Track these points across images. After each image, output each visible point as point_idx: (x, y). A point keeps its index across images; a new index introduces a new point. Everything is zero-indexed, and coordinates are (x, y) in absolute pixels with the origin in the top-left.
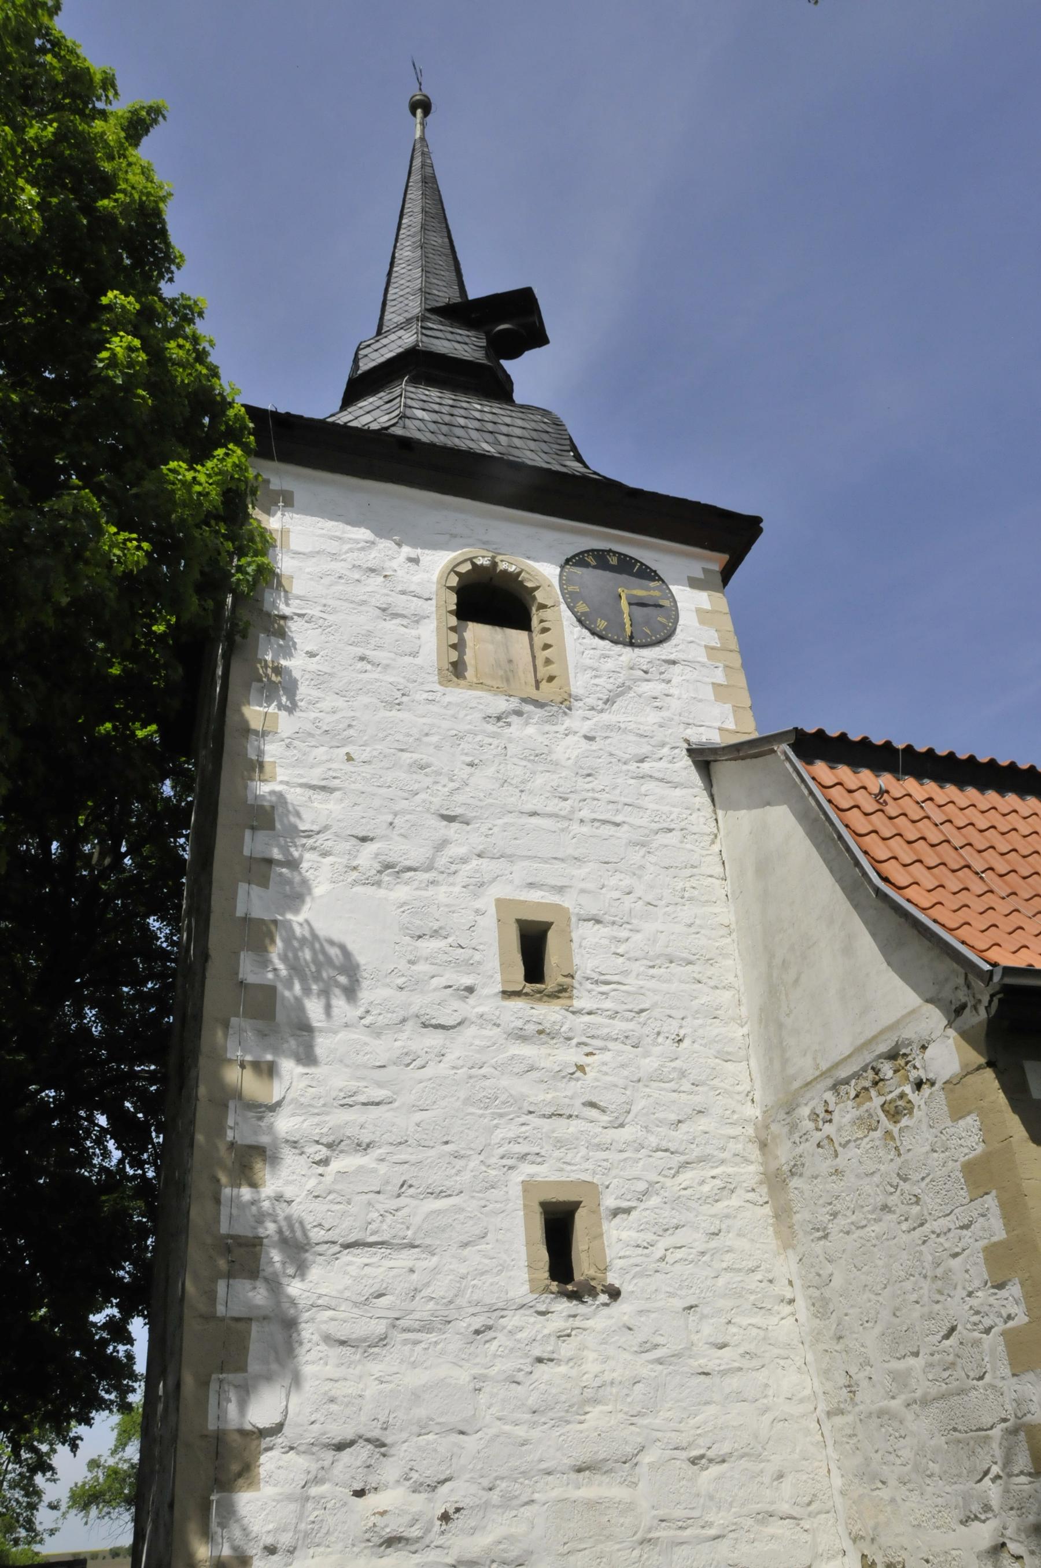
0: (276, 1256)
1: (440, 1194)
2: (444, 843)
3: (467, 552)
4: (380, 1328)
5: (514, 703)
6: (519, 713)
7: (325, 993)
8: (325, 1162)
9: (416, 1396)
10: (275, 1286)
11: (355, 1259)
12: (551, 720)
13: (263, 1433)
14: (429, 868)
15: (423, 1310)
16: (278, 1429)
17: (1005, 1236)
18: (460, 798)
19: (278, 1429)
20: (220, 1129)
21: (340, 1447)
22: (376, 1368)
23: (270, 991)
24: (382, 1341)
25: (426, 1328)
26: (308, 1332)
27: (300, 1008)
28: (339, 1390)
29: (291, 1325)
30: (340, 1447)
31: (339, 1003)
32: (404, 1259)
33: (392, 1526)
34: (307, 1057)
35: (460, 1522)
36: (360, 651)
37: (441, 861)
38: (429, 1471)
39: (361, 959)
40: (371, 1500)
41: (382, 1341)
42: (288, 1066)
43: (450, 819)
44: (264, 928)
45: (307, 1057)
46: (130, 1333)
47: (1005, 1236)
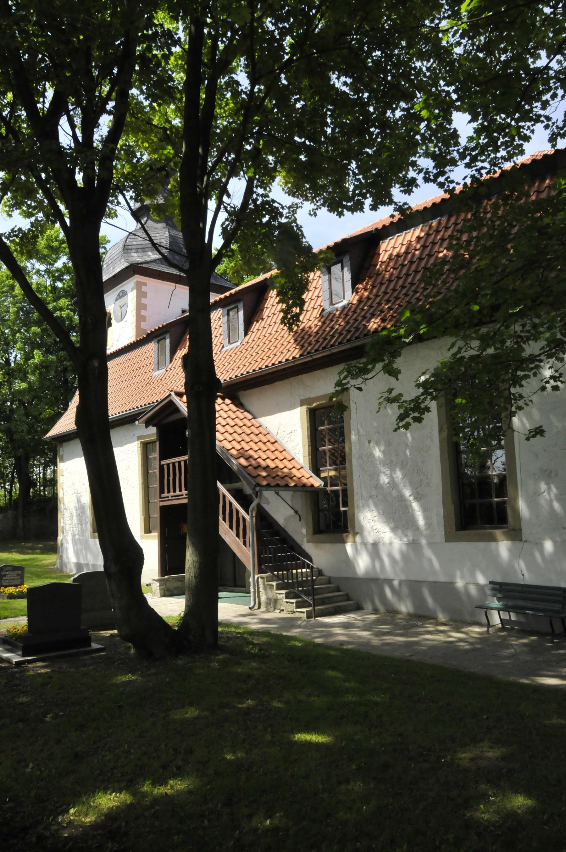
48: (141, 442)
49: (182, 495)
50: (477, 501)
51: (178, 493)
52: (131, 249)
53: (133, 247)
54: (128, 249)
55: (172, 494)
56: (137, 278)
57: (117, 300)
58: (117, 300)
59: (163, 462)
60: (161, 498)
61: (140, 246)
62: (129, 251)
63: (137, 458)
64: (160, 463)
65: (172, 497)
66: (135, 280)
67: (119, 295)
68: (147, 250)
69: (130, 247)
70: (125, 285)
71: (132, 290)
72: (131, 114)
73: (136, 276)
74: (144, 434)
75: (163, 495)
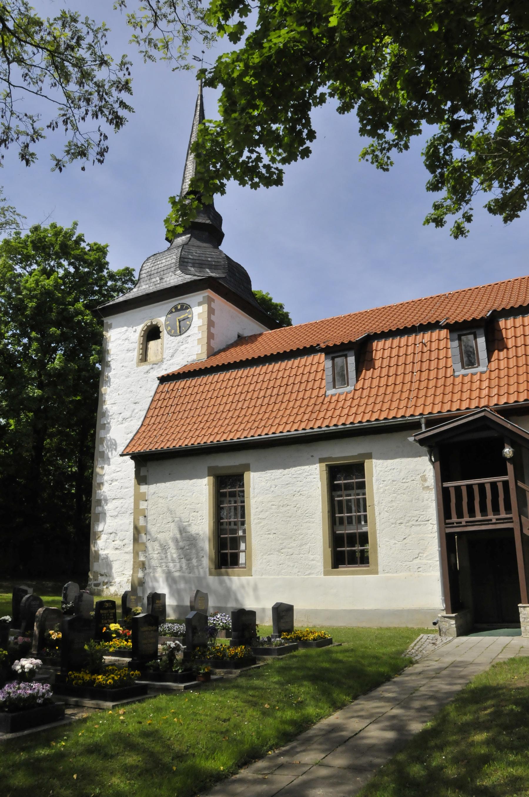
0: (103, 502)
1: (127, 488)
2: (134, 410)
3: (146, 323)
4: (116, 513)
5: (151, 366)
6: (152, 368)
7: (112, 451)
8: (111, 484)
9: (121, 525)
10: (103, 507)
11: (114, 501)
12: (159, 367)
13: (101, 532)
14: (131, 417)
15: (123, 510)
16: (103, 531)
17: (366, 461)
18: (138, 397)
19: (103, 531)
20: (96, 481)
21: (111, 534)
22: (116, 521)
23: (103, 452)
24: (117, 516)
25: (123, 513)
26: (108, 515)
27: (108, 454)
28: (111, 524)
29: (105, 514)
30: (111, 534)
31: (114, 452)
32: (121, 501)
33: (117, 546)
34: (109, 465)
35: (126, 546)
36: (122, 365)
37: (133, 414)
38: (122, 538)
39: (117, 442)
40: (115, 542)
41: (117, 516)
42: (106, 466)
43: (135, 403)
44: (32, 761)
45: (109, 465)
46: (308, 115)
47: (366, 461)
48: (327, 465)
49: (453, 523)
50: (228, 551)
51: (503, 515)
52: (187, 262)
53: (190, 261)
54: (184, 262)
55: (467, 518)
56: (208, 293)
57: (171, 312)
58: (171, 312)
59: (446, 485)
60: (446, 524)
61: (197, 262)
62: (185, 264)
63: (319, 484)
64: (442, 485)
65: (466, 522)
66: (206, 294)
67: (176, 307)
68: (204, 266)
69: (186, 260)
70: (187, 297)
71: (200, 304)
72: (497, 108)
73: (209, 290)
74: (333, 456)
75: (448, 521)
